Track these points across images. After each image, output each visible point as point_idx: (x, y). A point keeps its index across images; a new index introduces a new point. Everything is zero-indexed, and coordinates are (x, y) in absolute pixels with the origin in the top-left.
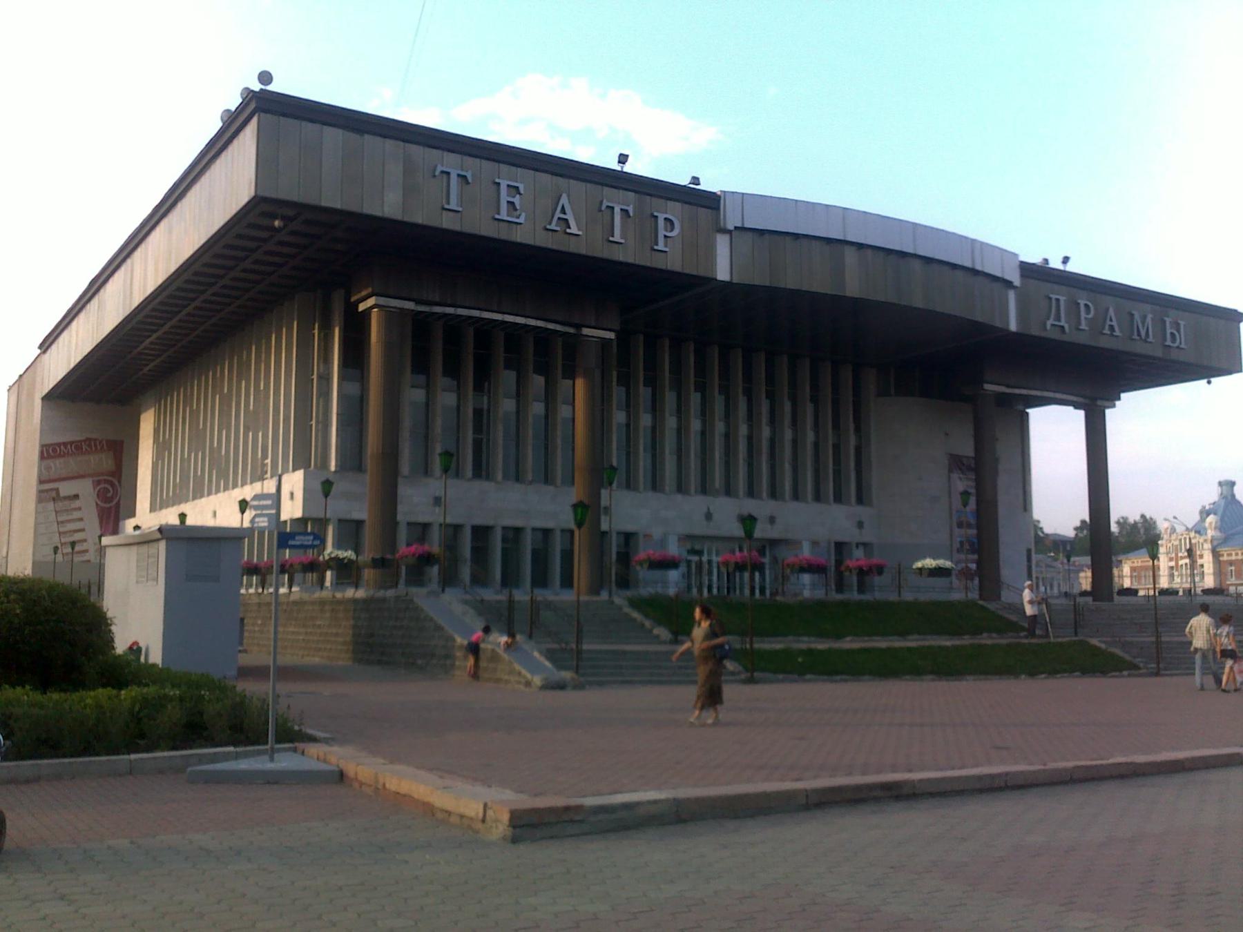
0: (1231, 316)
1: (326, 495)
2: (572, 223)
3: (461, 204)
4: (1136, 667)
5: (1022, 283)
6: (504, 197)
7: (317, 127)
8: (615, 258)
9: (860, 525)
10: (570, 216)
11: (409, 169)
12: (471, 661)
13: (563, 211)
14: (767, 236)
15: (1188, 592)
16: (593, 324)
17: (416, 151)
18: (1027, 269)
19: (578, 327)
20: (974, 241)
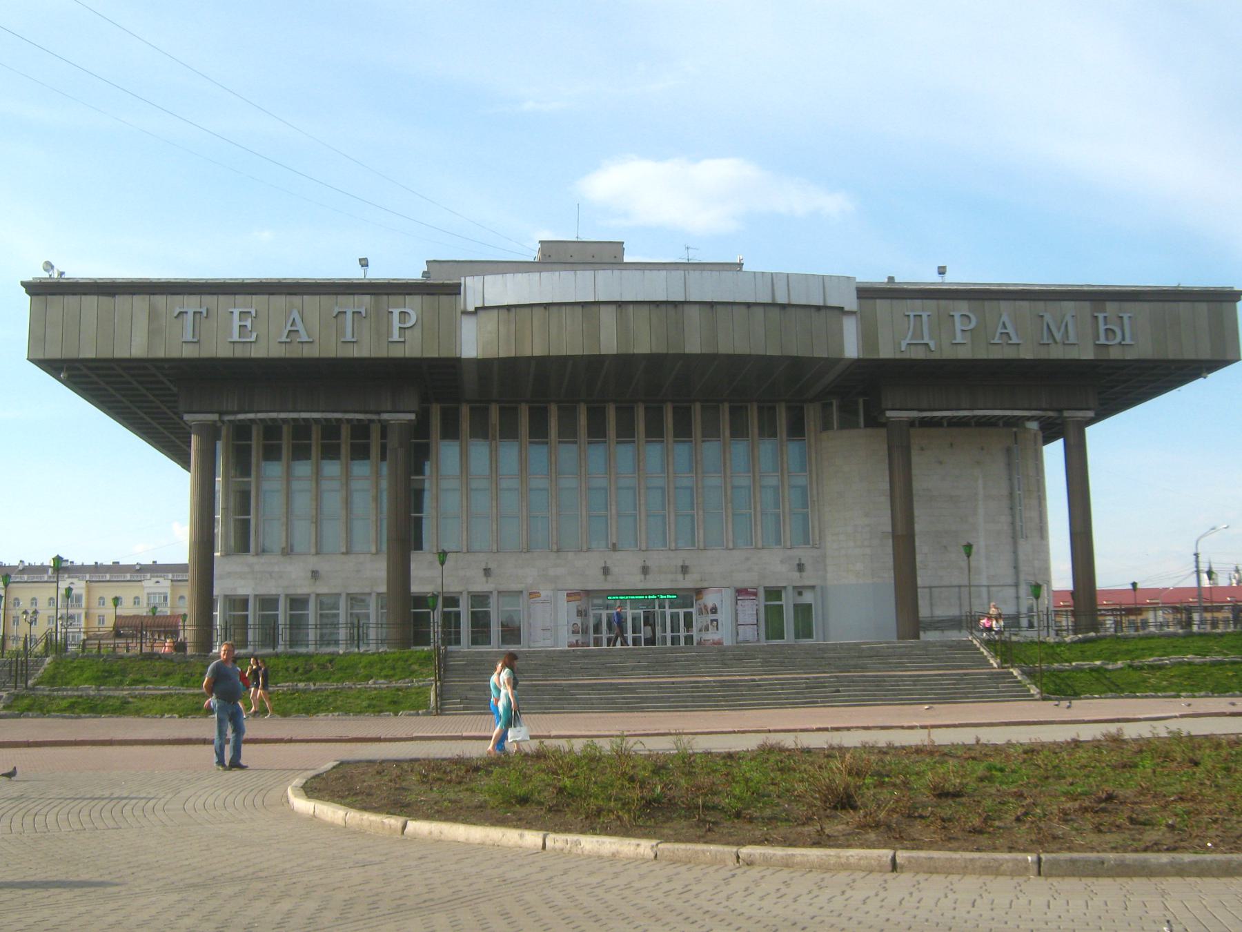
0: (1223, 298)
1: (116, 606)
2: (1012, 334)
3: (1132, 339)
4: (724, 758)
5: (860, 306)
6: (1102, 327)
7: (77, 297)
8: (253, 355)
9: (801, 567)
10: (1010, 330)
11: (153, 315)
12: (15, 795)
13: (1004, 326)
14: (823, 312)
15: (1074, 614)
16: (389, 408)
17: (160, 300)
18: (867, 293)
19: (1060, 410)
20: (772, 276)
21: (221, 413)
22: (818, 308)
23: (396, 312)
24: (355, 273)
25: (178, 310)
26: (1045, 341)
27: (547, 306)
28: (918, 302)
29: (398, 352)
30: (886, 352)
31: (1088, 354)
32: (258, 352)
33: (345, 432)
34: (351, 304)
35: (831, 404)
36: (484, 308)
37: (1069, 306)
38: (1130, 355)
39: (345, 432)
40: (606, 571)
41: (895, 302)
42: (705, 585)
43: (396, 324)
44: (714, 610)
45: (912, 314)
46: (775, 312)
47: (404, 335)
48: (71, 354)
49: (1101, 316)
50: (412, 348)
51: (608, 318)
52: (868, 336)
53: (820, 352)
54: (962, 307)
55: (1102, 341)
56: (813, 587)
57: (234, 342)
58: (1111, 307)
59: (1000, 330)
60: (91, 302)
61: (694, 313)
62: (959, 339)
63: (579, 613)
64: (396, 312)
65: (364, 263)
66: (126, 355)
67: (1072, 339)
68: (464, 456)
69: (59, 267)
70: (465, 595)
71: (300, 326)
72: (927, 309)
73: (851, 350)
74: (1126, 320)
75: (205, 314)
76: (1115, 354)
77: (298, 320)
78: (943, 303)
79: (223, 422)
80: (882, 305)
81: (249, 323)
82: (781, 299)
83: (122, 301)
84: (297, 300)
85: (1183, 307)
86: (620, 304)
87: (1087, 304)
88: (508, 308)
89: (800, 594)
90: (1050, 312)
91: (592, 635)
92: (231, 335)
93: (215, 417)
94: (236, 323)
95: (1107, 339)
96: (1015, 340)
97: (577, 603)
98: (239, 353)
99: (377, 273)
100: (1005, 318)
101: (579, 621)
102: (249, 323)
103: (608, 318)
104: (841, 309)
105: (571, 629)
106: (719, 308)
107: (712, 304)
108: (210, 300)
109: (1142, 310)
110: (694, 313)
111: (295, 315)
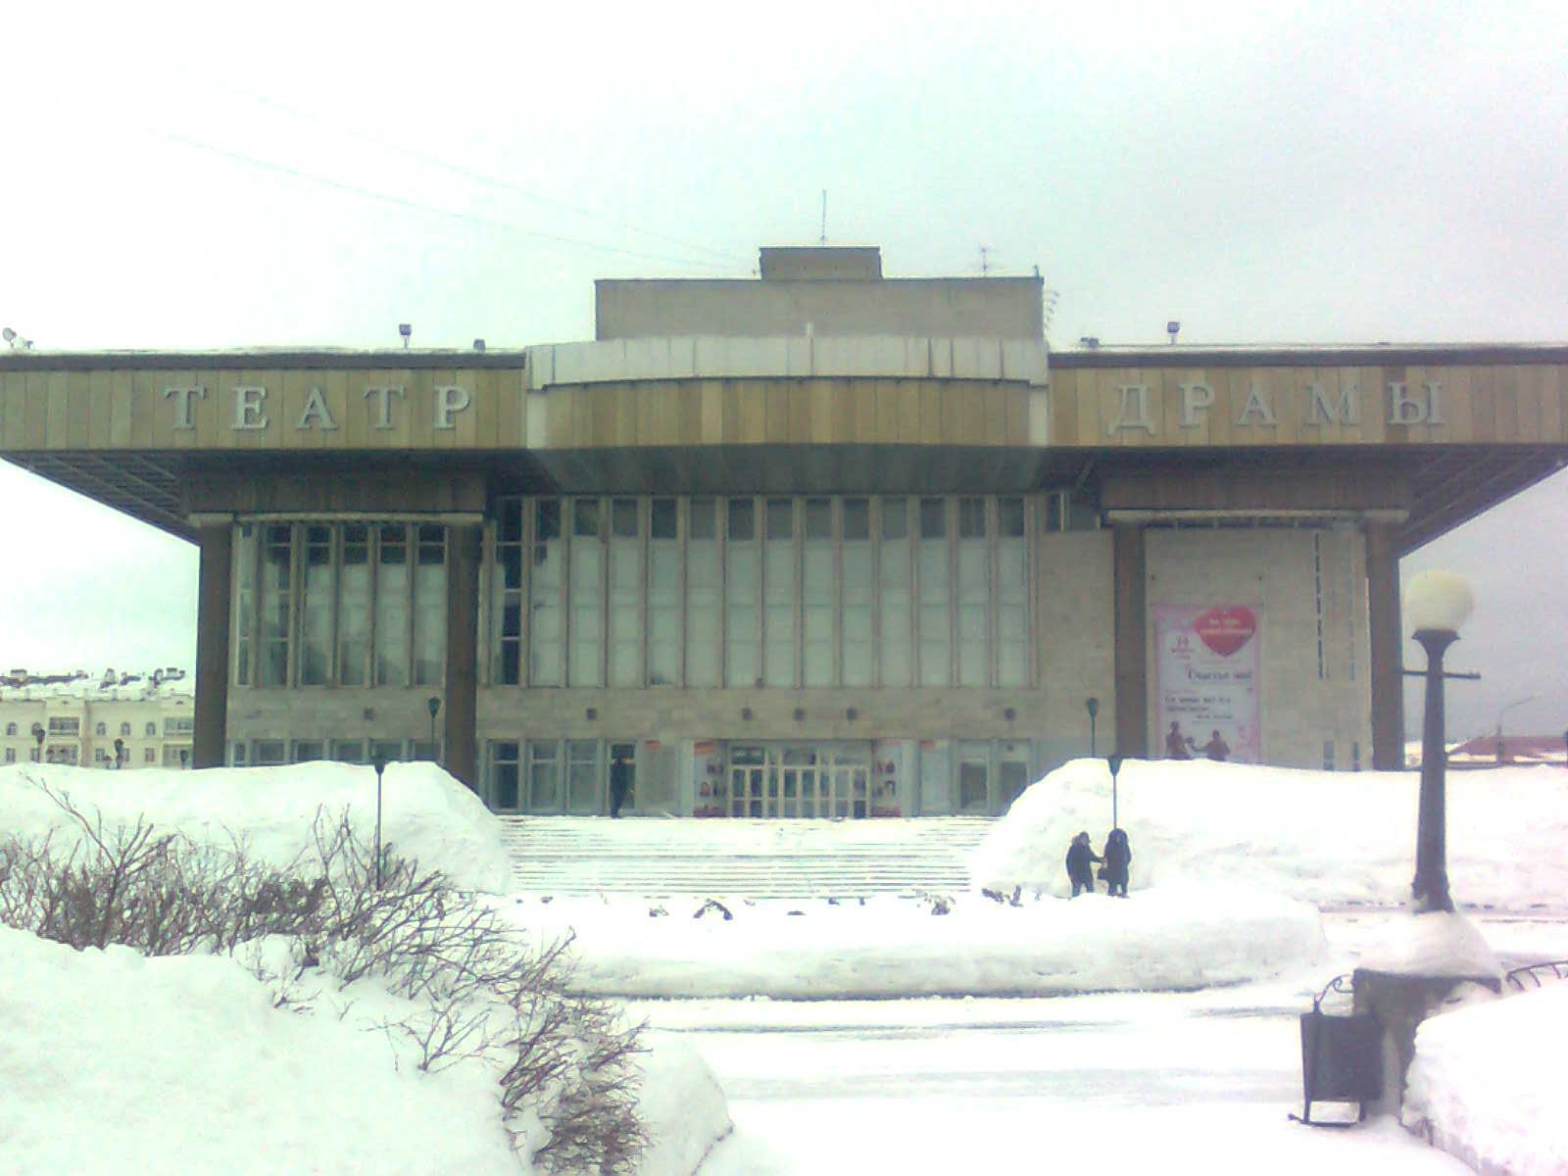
6: (1398, 402)
10: (1266, 409)
16: (448, 508)
21: (235, 513)
22: (996, 382)
23: (443, 392)
24: (393, 344)
25: (168, 390)
26: (1314, 420)
27: (632, 383)
28: (1134, 372)
29: (446, 442)
30: (1087, 439)
31: (1377, 437)
32: (267, 442)
33: (411, 534)
34: (382, 382)
35: (1058, 496)
36: (554, 386)
37: (1351, 374)
38: (1440, 438)
39: (411, 534)
40: (747, 714)
41: (288, 374)
42: (882, 734)
43: (443, 406)
44: (891, 768)
45: (1125, 389)
46: (932, 390)
47: (453, 421)
48: (79, 441)
49: (1397, 387)
50: (466, 436)
51: (711, 398)
52: (1063, 418)
53: (996, 440)
54: (1197, 377)
55: (1397, 418)
56: (1028, 741)
57: (239, 430)
58: (1414, 374)
59: (1248, 407)
60: (59, 379)
61: (824, 392)
62: (1189, 420)
63: (711, 769)
64: (443, 392)
65: (405, 331)
66: (104, 446)
67: (1353, 416)
68: (607, 560)
69: (23, 334)
70: (561, 743)
71: (321, 409)
72: (1147, 382)
73: (1040, 433)
74: (1434, 391)
75: (201, 393)
76: (1416, 437)
77: (319, 403)
78: (1170, 372)
79: (238, 523)
80: (1085, 377)
81: (256, 406)
82: (942, 371)
83: (99, 379)
84: (317, 376)
85: (1521, 373)
86: (727, 381)
87: (1377, 371)
88: (586, 385)
89: (1010, 748)
90: (1319, 383)
91: (731, 797)
92: (242, 422)
93: (228, 518)
94: (241, 407)
95: (1405, 415)
96: (1269, 419)
97: (706, 757)
98: (246, 443)
99: (423, 342)
100: (1257, 391)
101: (709, 780)
102: (256, 406)
103: (711, 398)
104: (1026, 383)
105: (699, 790)
106: (741, 386)
107: (849, 380)
108: (207, 377)
109: (1460, 376)
110: (824, 394)
111: (315, 395)
